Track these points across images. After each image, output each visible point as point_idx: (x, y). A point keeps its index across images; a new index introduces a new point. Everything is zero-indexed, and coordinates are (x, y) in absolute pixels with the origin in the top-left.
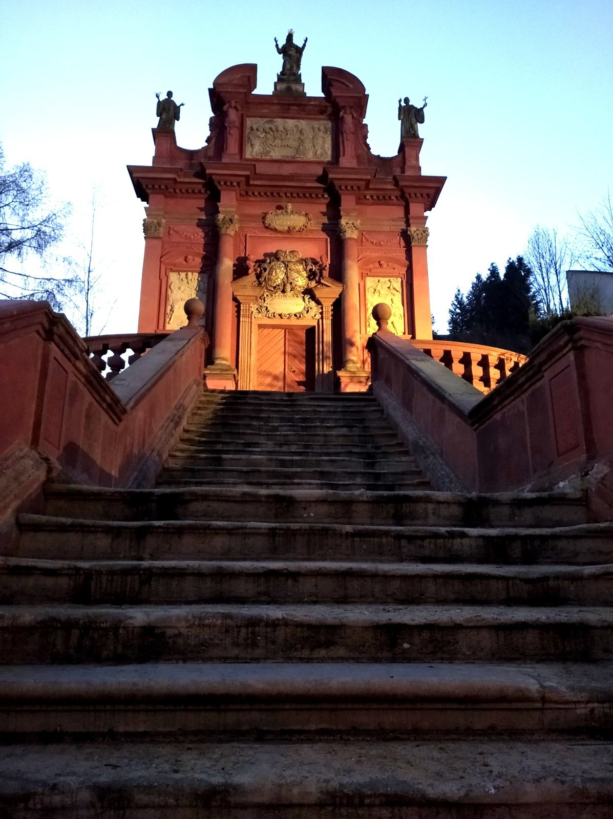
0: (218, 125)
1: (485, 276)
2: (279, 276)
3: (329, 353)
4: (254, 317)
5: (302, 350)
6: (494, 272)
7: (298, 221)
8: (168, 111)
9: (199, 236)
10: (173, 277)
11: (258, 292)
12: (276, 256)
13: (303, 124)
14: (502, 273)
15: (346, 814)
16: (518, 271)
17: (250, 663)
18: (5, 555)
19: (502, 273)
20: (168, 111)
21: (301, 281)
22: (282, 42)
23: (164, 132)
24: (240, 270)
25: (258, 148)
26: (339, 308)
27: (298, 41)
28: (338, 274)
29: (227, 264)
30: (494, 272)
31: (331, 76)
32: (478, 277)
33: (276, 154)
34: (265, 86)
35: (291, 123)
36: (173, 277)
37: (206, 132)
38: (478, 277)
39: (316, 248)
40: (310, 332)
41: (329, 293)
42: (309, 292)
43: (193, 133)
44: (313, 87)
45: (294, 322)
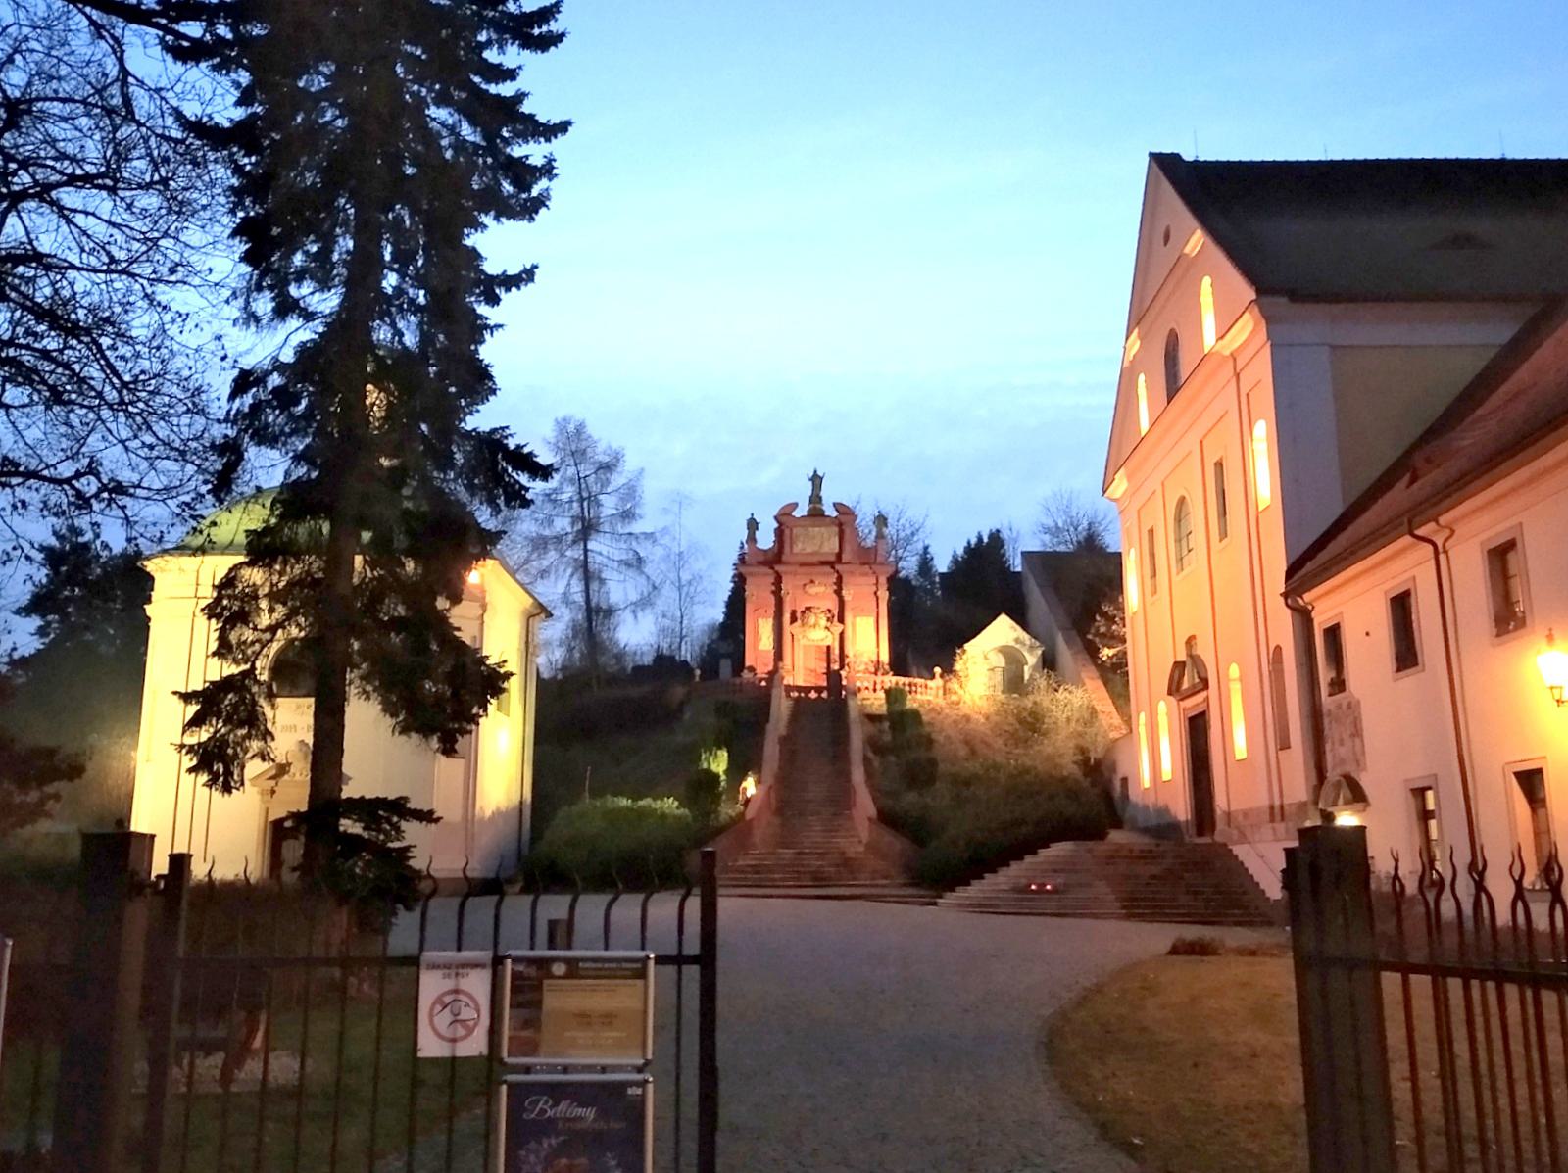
0: (779, 533)
1: (974, 541)
2: (812, 620)
3: (838, 659)
4: (801, 642)
5: (825, 656)
6: (980, 539)
7: (822, 589)
8: (753, 525)
9: (772, 599)
10: (760, 621)
11: (801, 629)
12: (809, 608)
13: (823, 529)
14: (986, 540)
15: (426, 207)
16: (996, 538)
17: (1279, 957)
18: (1394, 1164)
19: (986, 540)
20: (753, 525)
21: (823, 622)
22: (811, 474)
23: (752, 539)
24: (793, 620)
25: (800, 545)
26: (842, 635)
27: (820, 474)
28: (841, 620)
29: (787, 617)
30: (980, 539)
31: (837, 506)
32: (969, 543)
33: (809, 550)
34: (801, 512)
35: (817, 529)
36: (760, 621)
37: (773, 538)
38: (969, 543)
39: (832, 603)
40: (828, 647)
41: (837, 628)
42: (827, 628)
43: (766, 540)
44: (831, 512)
45: (821, 643)
